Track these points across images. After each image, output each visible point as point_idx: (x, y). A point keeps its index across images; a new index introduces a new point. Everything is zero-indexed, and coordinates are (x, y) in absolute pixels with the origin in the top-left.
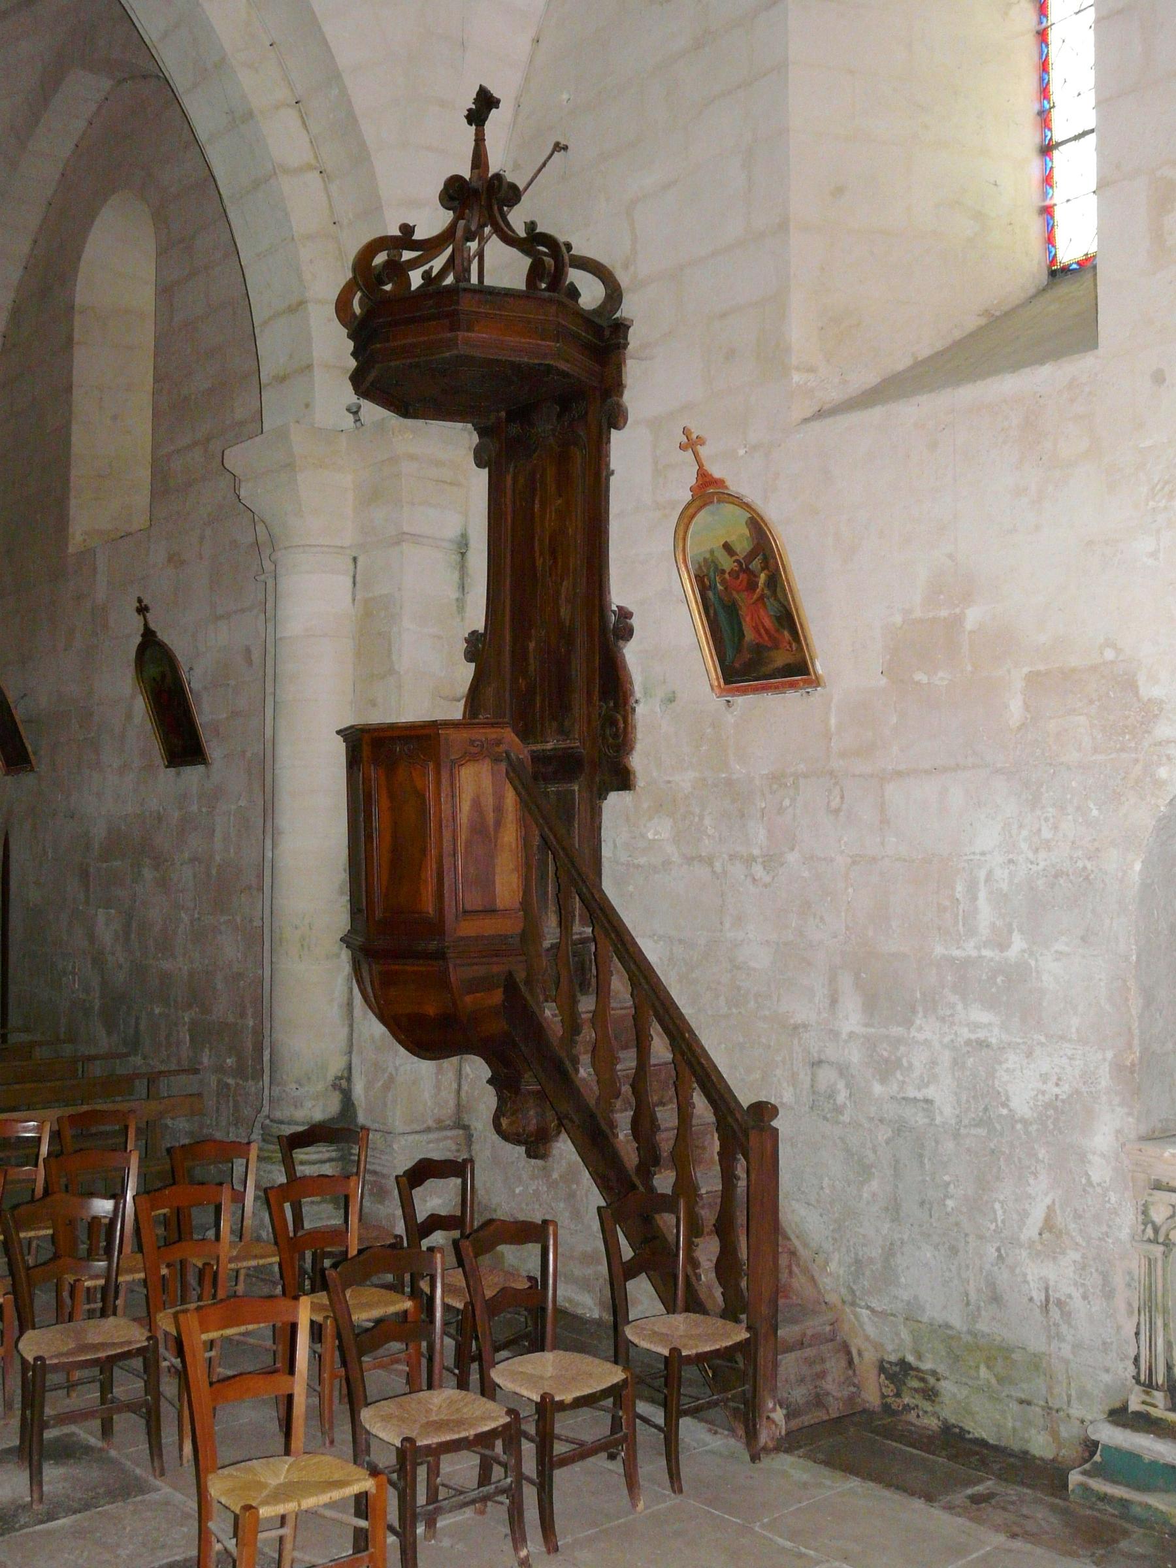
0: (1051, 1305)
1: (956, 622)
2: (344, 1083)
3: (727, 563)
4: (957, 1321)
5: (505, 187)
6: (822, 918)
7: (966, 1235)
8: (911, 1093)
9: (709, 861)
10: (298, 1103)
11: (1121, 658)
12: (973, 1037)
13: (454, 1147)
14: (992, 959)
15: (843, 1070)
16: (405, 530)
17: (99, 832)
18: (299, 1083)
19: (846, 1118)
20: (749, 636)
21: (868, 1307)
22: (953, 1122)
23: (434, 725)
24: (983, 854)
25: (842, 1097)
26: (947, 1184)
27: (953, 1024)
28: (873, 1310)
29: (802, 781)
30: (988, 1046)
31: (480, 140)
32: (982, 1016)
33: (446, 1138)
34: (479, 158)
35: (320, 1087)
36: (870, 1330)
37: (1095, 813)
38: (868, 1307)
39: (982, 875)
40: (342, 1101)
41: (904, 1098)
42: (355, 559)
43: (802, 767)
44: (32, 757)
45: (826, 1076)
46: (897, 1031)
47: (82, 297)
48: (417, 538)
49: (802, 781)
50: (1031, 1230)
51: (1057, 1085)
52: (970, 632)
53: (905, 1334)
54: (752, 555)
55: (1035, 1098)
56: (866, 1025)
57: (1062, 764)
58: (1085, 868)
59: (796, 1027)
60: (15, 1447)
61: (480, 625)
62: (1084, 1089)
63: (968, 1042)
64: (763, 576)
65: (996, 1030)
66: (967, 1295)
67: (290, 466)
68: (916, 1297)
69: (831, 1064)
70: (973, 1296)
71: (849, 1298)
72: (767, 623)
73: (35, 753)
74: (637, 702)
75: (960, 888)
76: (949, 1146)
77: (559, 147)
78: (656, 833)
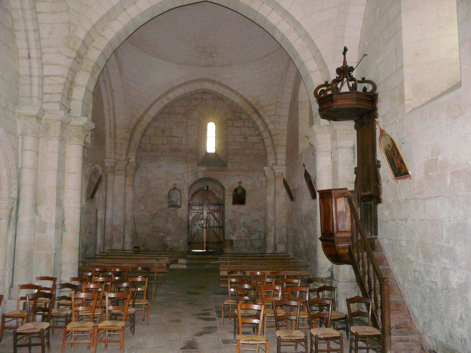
0: (462, 340)
1: (437, 159)
2: (331, 270)
3: (390, 149)
4: (444, 341)
5: (348, 68)
6: (415, 234)
7: (445, 319)
8: (433, 280)
9: (395, 220)
10: (321, 274)
11: (469, 167)
12: (444, 266)
13: (354, 286)
14: (446, 246)
15: (420, 273)
16: (338, 145)
17: (304, 214)
18: (321, 269)
19: (421, 285)
20: (397, 166)
21: (427, 335)
22: (441, 288)
23: (330, 190)
24: (444, 219)
25: (420, 280)
26: (441, 304)
27: (440, 262)
28: (428, 336)
29: (410, 201)
30: (447, 269)
31: (345, 58)
32: (446, 261)
33: (352, 284)
34: (345, 62)
35: (326, 270)
36: (428, 341)
37: (466, 208)
38: (427, 335)
39: (444, 224)
40: (331, 274)
41: (431, 281)
42: (331, 153)
43: (410, 197)
44: (294, 198)
45: (417, 274)
46: (429, 264)
47: (299, 100)
48: (342, 148)
49: (410, 201)
50: (457, 319)
51: (461, 280)
52: (440, 162)
53: (434, 344)
54: (393, 147)
55: (457, 283)
56: (424, 262)
57: (458, 195)
58: (464, 222)
59: (411, 262)
60: (138, 299)
61: (356, 166)
62: (467, 282)
63: (443, 267)
64: (396, 151)
65: (448, 265)
66: (446, 335)
67: (315, 134)
68: (436, 334)
69: (418, 271)
70: (447, 336)
71: (423, 332)
72: (399, 163)
73: (295, 197)
74: (382, 182)
75: (440, 227)
76: (440, 294)
77: (365, 55)
78: (386, 213)
